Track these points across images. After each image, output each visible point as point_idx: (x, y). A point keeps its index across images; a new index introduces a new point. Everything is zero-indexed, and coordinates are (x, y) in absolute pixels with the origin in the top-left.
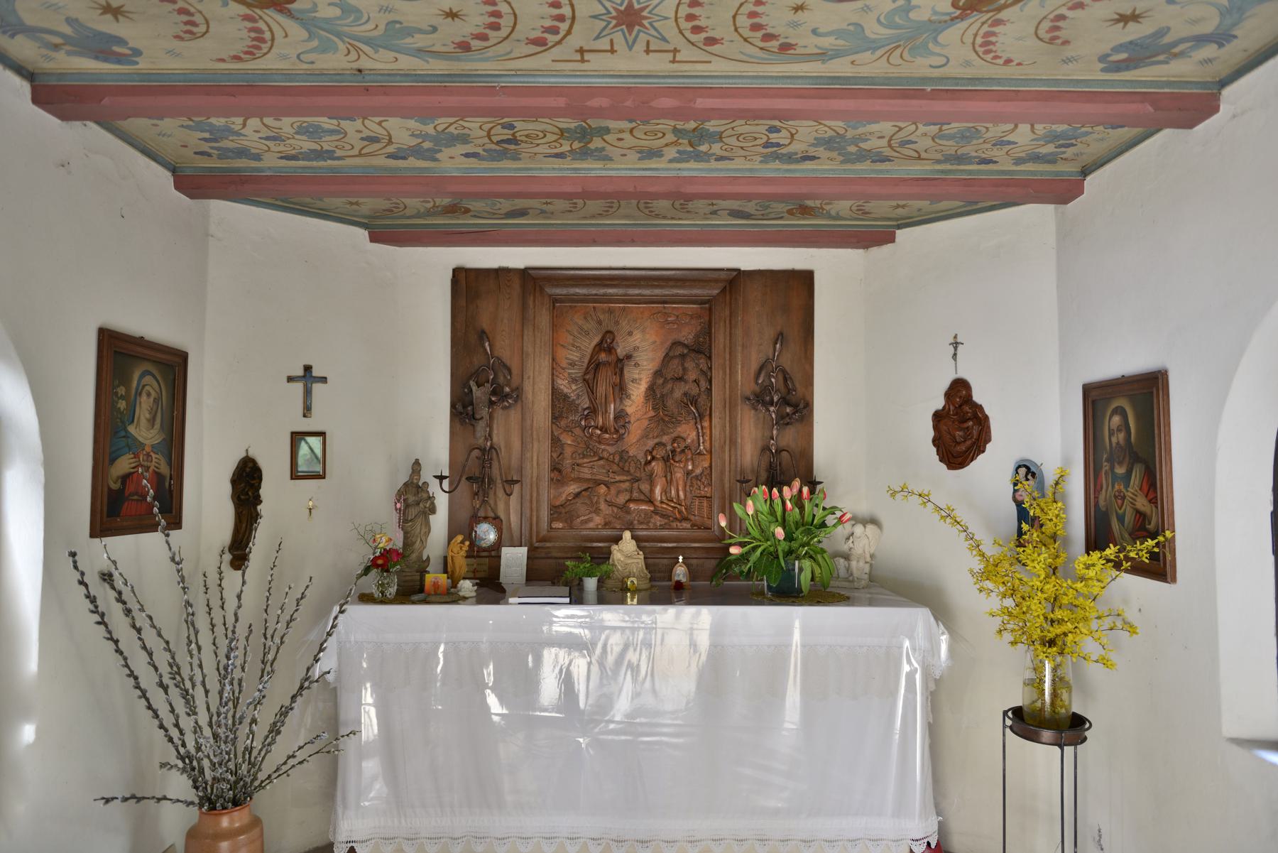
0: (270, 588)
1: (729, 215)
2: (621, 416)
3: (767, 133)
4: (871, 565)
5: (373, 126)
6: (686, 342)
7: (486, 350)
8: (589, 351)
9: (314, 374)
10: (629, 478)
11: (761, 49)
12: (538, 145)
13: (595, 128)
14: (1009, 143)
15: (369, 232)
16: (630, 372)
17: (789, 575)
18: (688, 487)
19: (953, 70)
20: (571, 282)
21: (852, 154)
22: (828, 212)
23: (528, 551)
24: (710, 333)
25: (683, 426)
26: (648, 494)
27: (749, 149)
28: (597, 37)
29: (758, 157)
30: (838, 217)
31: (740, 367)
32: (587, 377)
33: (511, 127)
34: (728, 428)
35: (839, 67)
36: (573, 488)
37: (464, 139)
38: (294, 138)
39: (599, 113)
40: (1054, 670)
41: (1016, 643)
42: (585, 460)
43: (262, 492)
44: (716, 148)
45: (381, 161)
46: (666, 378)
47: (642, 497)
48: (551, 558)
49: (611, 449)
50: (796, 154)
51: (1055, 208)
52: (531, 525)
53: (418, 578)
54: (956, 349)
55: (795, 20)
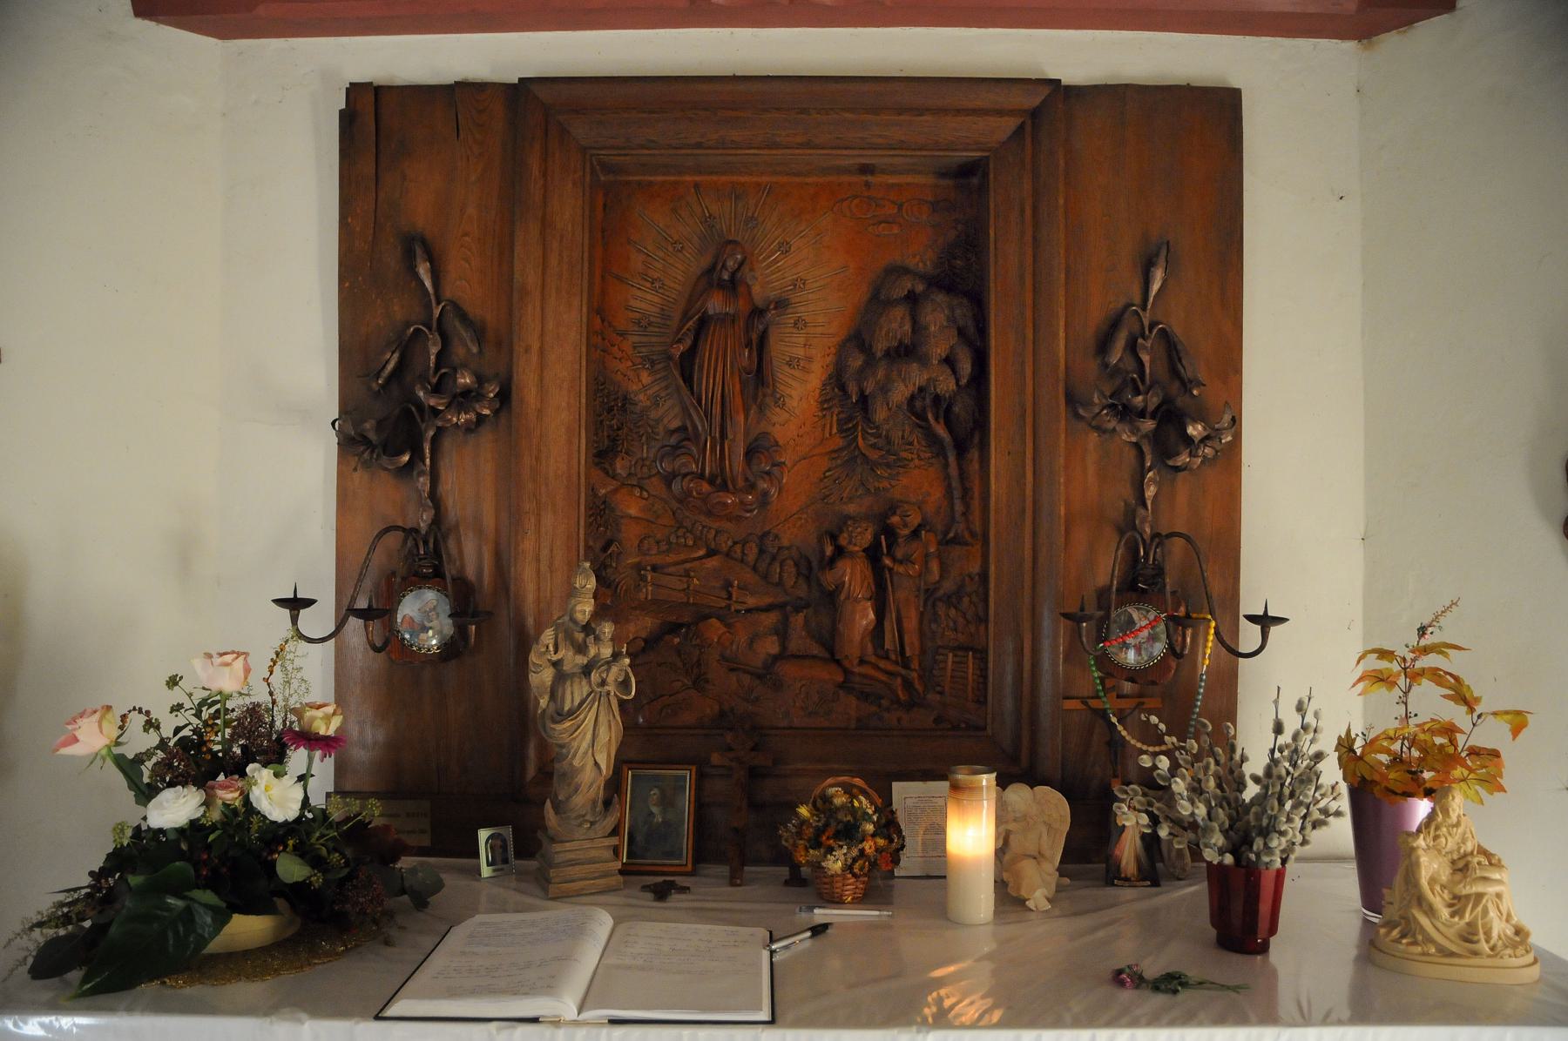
42: (671, 558)
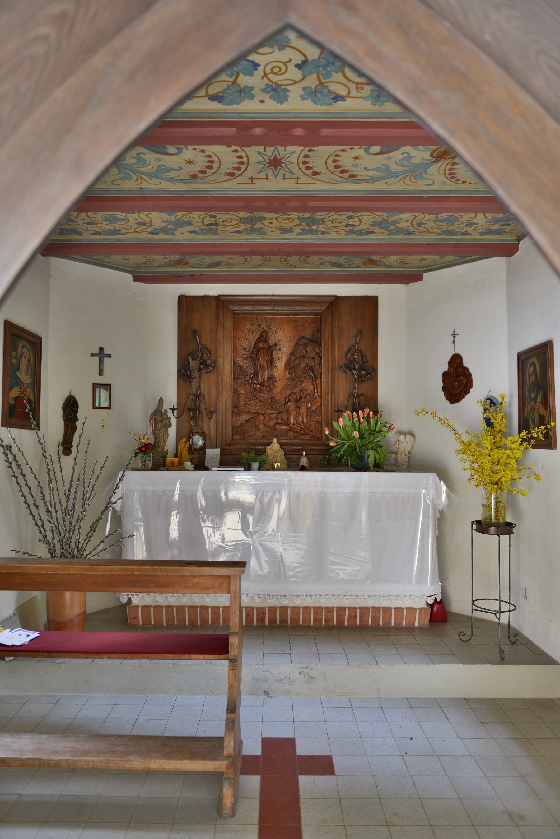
0: (85, 463)
1: (331, 265)
2: (271, 378)
3: (347, 219)
4: (409, 457)
5: (143, 216)
6: (307, 337)
7: (197, 341)
8: (254, 341)
9: (105, 352)
10: (276, 412)
11: (340, 177)
12: (228, 226)
13: (258, 217)
14: (475, 224)
15: (133, 276)
16: (277, 354)
17: (361, 458)
18: (308, 416)
19: (437, 187)
20: (243, 303)
21: (392, 230)
22: (385, 263)
23: (221, 451)
24: (321, 331)
25: (306, 383)
26: (287, 421)
27: (339, 228)
28: (260, 172)
29: (343, 232)
30: (390, 266)
31: (337, 349)
32: (253, 356)
33: (214, 217)
34: (330, 383)
35: (380, 186)
36: (245, 417)
37: (190, 223)
38: (101, 223)
39: (260, 209)
40: (497, 498)
41: (478, 485)
42: (252, 402)
43: (78, 415)
44: (321, 228)
45: (145, 235)
46: (296, 357)
47: (283, 422)
48: (233, 454)
49: (266, 396)
50: (363, 230)
51: (506, 260)
52: (222, 437)
53: (162, 461)
54: (454, 338)
55: (356, 163)
